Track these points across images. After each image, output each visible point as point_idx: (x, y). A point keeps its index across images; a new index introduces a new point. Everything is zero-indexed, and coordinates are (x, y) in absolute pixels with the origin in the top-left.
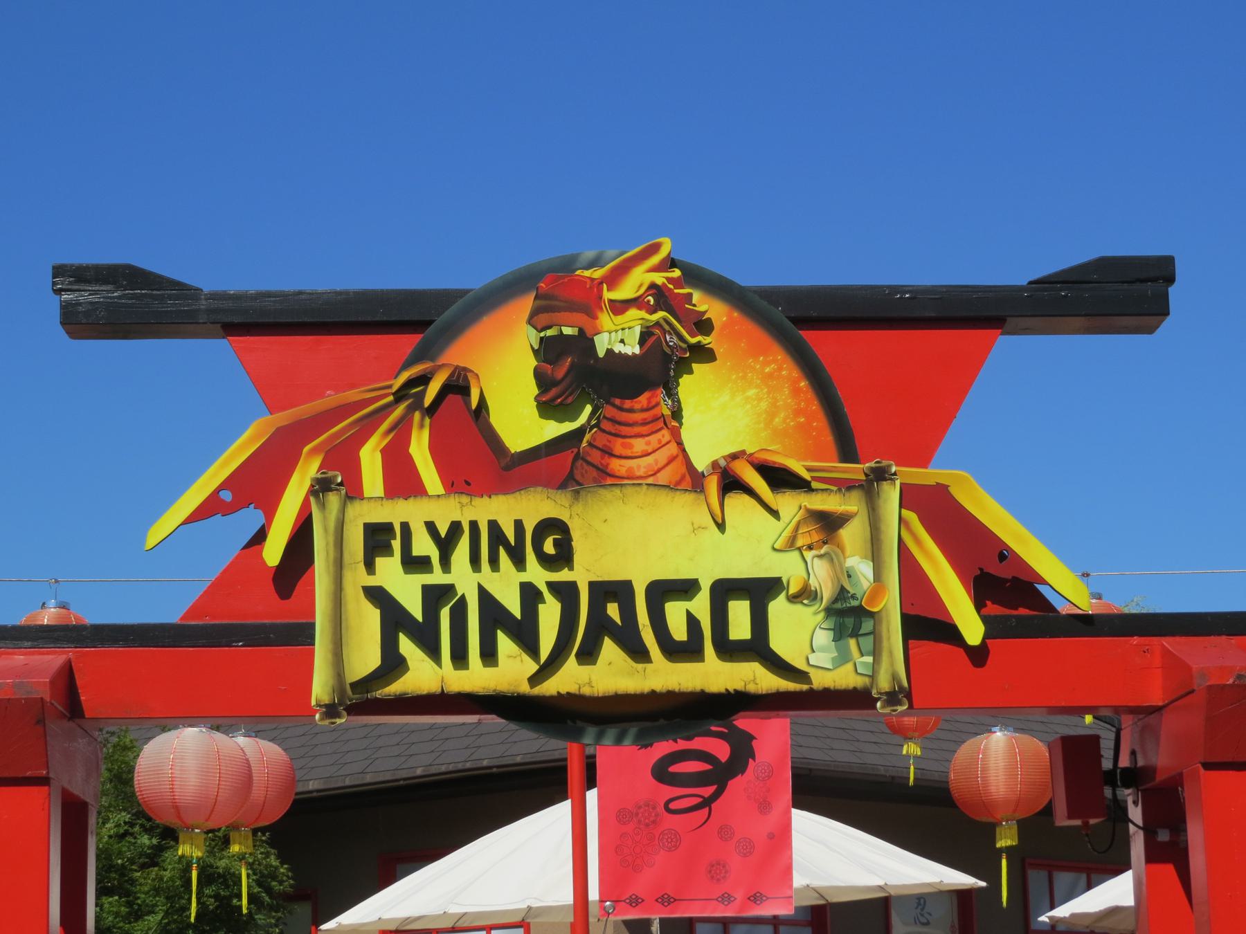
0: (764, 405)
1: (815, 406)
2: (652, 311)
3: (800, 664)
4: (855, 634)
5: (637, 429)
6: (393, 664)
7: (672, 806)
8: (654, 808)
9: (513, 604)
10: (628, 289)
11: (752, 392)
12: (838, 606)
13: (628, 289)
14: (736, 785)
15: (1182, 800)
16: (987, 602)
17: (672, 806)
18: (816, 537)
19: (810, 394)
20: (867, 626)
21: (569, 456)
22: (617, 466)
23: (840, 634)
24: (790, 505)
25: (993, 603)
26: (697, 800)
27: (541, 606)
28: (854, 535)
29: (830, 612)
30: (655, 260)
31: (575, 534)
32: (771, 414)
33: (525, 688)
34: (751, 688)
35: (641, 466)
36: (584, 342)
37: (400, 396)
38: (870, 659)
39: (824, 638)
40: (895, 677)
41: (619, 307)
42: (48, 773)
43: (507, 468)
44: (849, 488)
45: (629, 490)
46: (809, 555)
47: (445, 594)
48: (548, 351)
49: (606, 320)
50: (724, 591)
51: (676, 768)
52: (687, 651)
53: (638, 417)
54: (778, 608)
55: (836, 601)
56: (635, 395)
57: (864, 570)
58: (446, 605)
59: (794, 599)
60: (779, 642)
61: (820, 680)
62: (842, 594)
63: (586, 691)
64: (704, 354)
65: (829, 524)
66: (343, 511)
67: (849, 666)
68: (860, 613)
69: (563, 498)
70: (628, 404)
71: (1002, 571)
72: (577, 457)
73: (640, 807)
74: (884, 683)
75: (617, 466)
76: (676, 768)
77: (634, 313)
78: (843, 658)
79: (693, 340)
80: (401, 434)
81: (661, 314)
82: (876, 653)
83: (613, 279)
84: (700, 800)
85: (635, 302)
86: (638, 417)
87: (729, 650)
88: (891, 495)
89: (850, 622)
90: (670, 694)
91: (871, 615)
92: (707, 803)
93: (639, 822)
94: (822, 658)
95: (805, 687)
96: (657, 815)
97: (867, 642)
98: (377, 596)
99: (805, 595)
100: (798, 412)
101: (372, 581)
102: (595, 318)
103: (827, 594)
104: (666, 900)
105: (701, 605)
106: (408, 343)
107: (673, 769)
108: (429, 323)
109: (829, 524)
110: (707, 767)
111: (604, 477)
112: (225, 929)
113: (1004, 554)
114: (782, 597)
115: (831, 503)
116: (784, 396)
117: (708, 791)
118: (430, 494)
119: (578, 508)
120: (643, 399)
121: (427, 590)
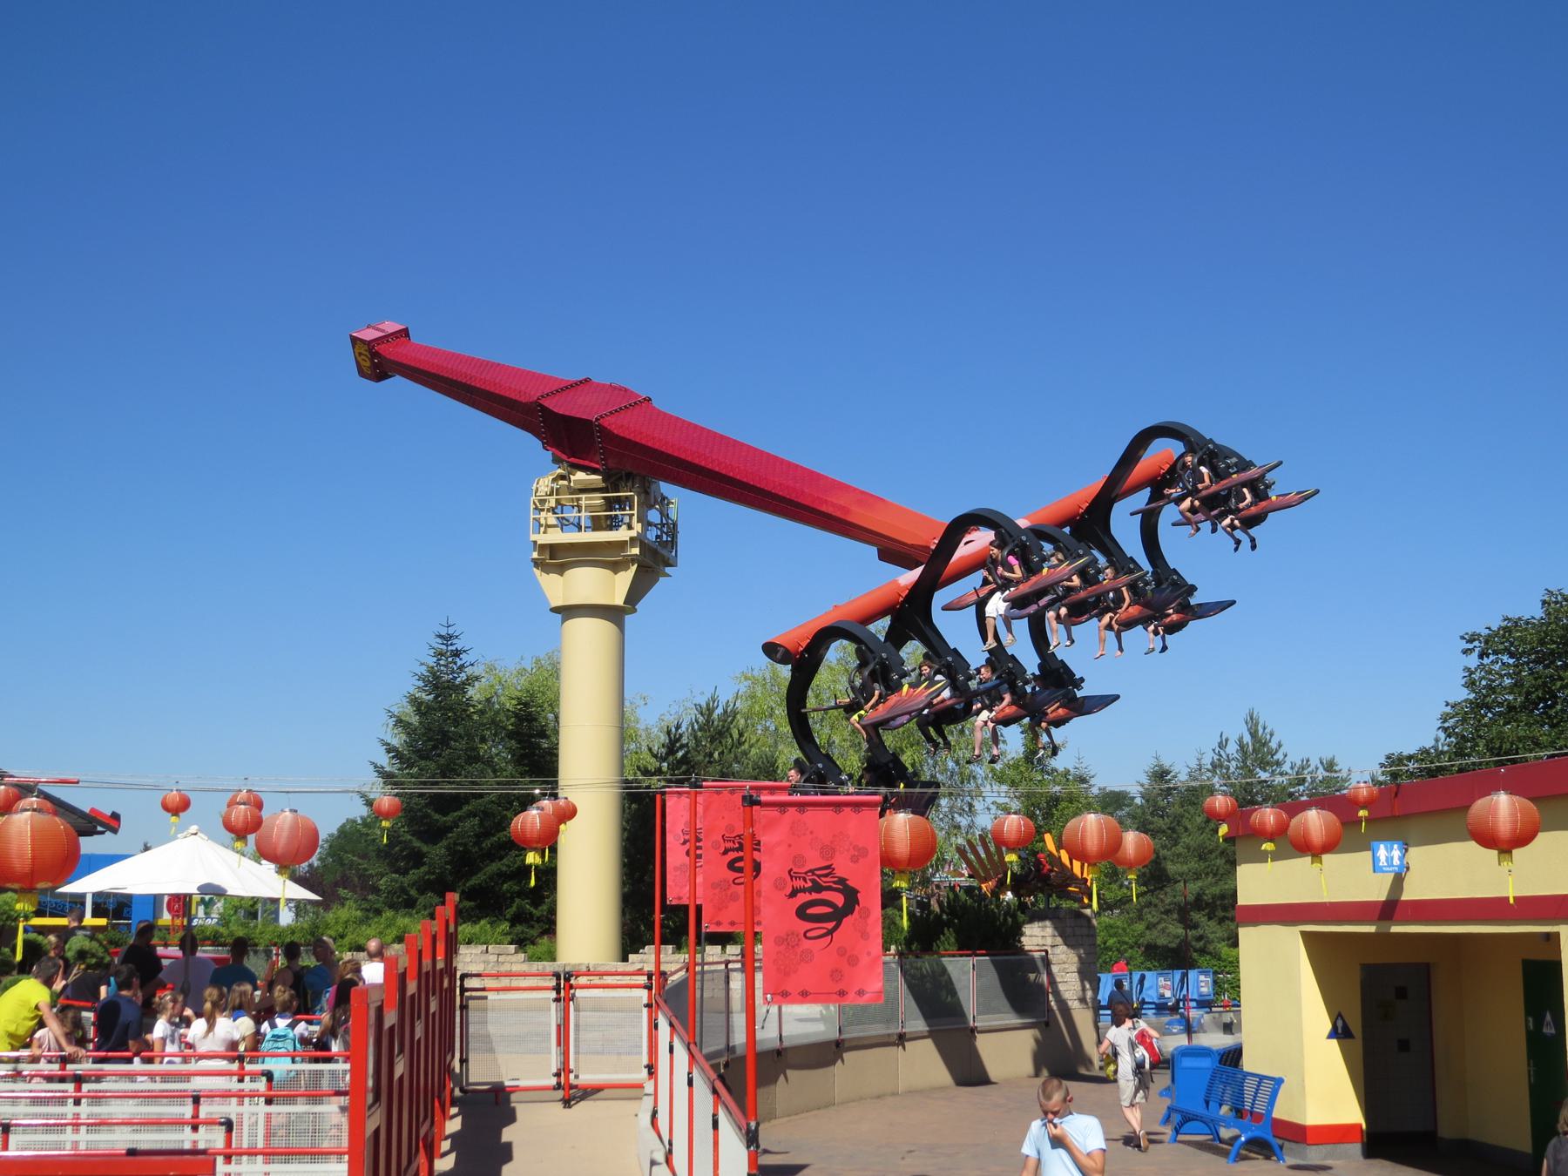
7: (736, 881)
8: (797, 936)
14: (848, 922)
15: (1531, 1061)
16: (1263, 848)
17: (736, 881)
27: (1310, 858)
42: (983, 666)
47: (910, 1092)
51: (811, 911)
58: (162, 911)
73: (788, 935)
76: (811, 911)
84: (825, 931)
92: (830, 932)
93: (788, 944)
96: (799, 940)
107: (809, 911)
110: (831, 910)
112: (479, 901)
117: (830, 925)
118: (758, 1090)
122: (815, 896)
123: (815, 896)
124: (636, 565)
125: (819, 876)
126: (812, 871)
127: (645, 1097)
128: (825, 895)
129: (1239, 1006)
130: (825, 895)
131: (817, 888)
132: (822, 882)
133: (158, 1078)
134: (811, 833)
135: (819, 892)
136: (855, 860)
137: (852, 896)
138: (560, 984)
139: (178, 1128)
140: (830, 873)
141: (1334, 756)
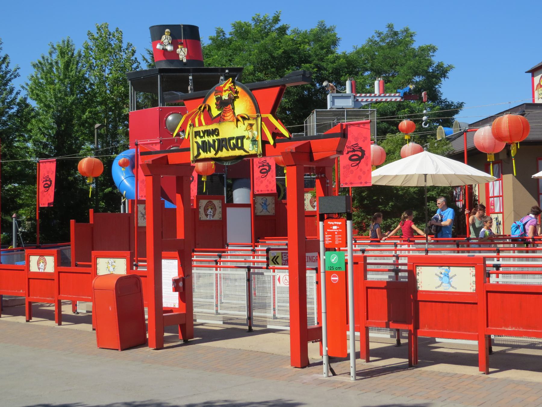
0: (246, 105)
1: (253, 105)
2: (229, 91)
3: (248, 150)
4: (255, 144)
5: (228, 112)
6: (199, 154)
7: (352, 165)
9: (211, 142)
10: (226, 88)
11: (244, 103)
12: (253, 140)
13: (226, 88)
14: (362, 160)
17: (352, 165)
18: (250, 128)
19: (252, 103)
20: (256, 143)
21: (220, 117)
22: (226, 118)
23: (253, 144)
24: (247, 122)
25: (454, 116)
26: (356, 164)
28: (254, 127)
29: (252, 141)
30: (230, 82)
31: (220, 131)
32: (246, 107)
33: (214, 156)
34: (242, 155)
35: (228, 118)
36: (221, 97)
37: (199, 109)
38: (257, 149)
39: (251, 145)
40: (260, 152)
41: (225, 91)
43: (212, 120)
44: (254, 119)
45: (226, 122)
46: (249, 131)
48: (217, 99)
49: (224, 93)
50: (237, 138)
51: (353, 158)
52: (233, 149)
53: (228, 109)
54: (245, 140)
55: (252, 139)
56: (227, 106)
57: (256, 133)
59: (247, 139)
60: (245, 147)
61: (251, 153)
62: (253, 138)
63: (222, 156)
64: (237, 97)
65: (251, 125)
66: (193, 129)
67: (254, 150)
68: (256, 141)
69: (218, 124)
70: (227, 107)
71: (275, 131)
72: (221, 117)
74: (259, 153)
75: (226, 118)
76: (353, 158)
77: (227, 92)
78: (253, 149)
79: (234, 95)
80: (200, 115)
81: (231, 91)
82: (258, 147)
83: (224, 86)
85: (227, 90)
86: (228, 109)
87: (239, 149)
88: (259, 119)
89: (254, 142)
90: (232, 156)
91: (257, 141)
92: (358, 164)
94: (251, 149)
95: (248, 154)
97: (256, 145)
98: (197, 142)
99: (248, 138)
100: (250, 106)
101: (196, 140)
102: (222, 93)
103: (251, 138)
104: (351, 183)
105: (234, 141)
106: (203, 99)
107: (262, 171)
108: (205, 97)
109: (251, 125)
111: (224, 120)
113: (276, 128)
114: (245, 139)
115: (251, 122)
116: (248, 103)
117: (358, 162)
119: (220, 126)
120: (228, 106)
121: (202, 141)
122: (354, 153)
123: (354, 153)
124: (100, 125)
125: (354, 147)
126: (352, 145)
127: (262, 209)
128: (356, 153)
129: (426, 175)
130: (356, 153)
131: (263, 166)
132: (356, 148)
133: (516, 251)
134: (352, 133)
135: (354, 152)
136: (364, 141)
137: (270, 167)
138: (227, 191)
139: (527, 276)
140: (357, 146)
141: (461, 105)
